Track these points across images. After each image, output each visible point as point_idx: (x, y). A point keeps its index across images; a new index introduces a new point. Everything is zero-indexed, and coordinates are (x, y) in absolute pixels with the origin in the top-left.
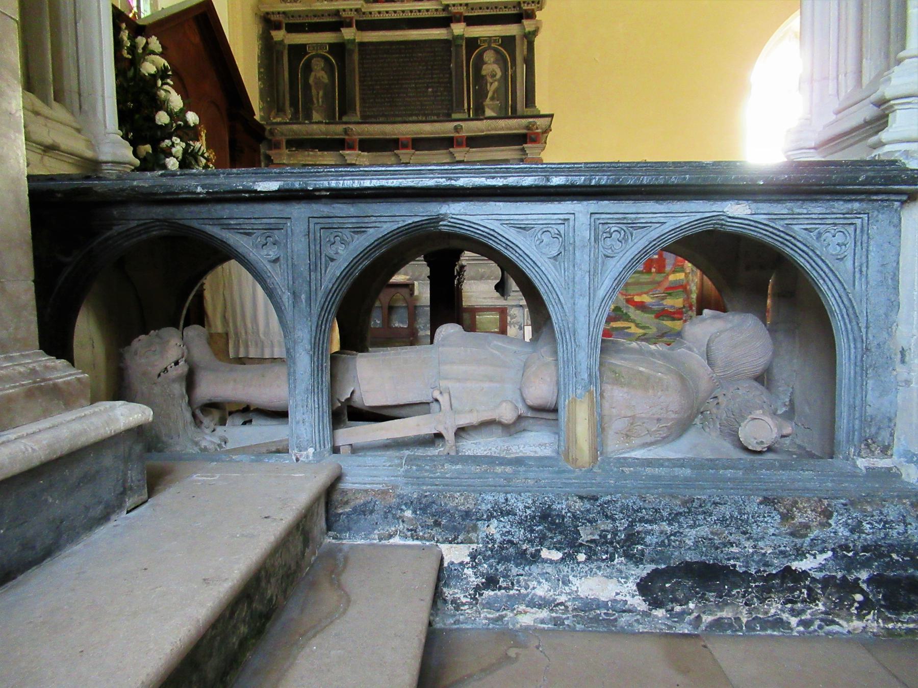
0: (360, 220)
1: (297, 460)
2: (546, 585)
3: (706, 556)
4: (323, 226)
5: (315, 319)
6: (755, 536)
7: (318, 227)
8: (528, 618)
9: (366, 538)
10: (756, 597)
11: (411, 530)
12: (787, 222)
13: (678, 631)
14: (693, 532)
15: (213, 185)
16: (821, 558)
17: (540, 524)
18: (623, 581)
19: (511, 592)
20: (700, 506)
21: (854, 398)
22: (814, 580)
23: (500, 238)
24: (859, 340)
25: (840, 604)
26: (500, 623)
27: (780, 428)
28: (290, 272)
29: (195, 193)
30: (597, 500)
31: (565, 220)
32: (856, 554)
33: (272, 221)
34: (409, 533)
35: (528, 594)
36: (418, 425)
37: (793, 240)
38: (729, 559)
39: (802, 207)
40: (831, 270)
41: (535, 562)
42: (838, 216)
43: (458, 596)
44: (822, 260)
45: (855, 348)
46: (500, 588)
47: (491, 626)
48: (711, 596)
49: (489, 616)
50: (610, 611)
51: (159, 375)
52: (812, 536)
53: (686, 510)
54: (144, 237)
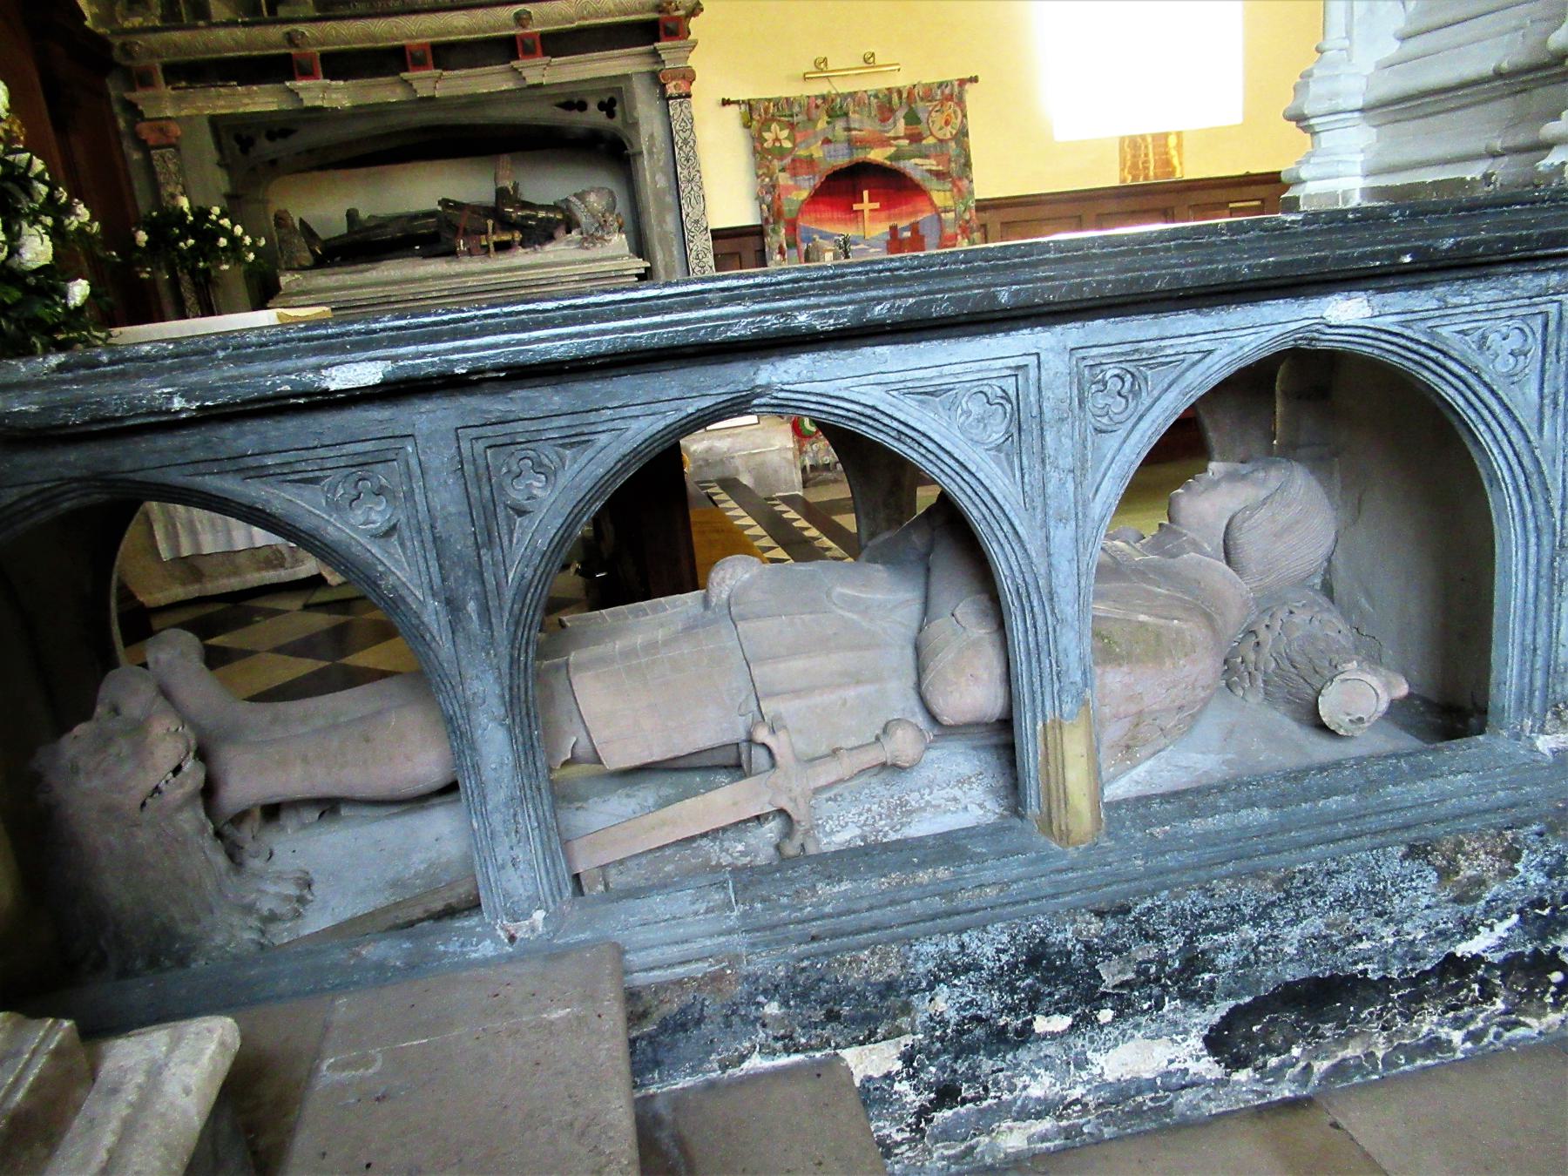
0: (576, 420)
1: (512, 939)
2: (1046, 1078)
3: (1319, 965)
4: (491, 442)
5: (504, 650)
6: (1398, 917)
7: (480, 446)
8: (1013, 1138)
9: (694, 1071)
10: (1400, 1013)
11: (783, 1038)
12: (1430, 323)
13: (1276, 1097)
14: (1297, 931)
15: (212, 390)
16: (1501, 929)
17: (1027, 973)
18: (1179, 1038)
19: (985, 1104)
20: (1306, 883)
21: (1535, 633)
22: (1491, 966)
23: (887, 420)
24: (1546, 530)
25: (1529, 995)
26: (969, 1159)
27: (1388, 686)
28: (432, 555)
29: (168, 412)
30: (1128, 911)
31: (1018, 368)
32: (1555, 909)
33: (369, 446)
34: (779, 1045)
35: (1015, 1100)
36: (735, 804)
37: (1441, 358)
38: (1355, 963)
39: (1460, 294)
40: (1507, 409)
41: (1024, 1043)
42: (1521, 302)
43: (886, 1132)
44: (1493, 392)
45: (1538, 545)
46: (964, 1101)
47: (954, 1168)
48: (1328, 1029)
49: (946, 1153)
50: (1161, 1093)
51: (143, 804)
52: (1488, 896)
53: (1282, 895)
54: (45, 515)
